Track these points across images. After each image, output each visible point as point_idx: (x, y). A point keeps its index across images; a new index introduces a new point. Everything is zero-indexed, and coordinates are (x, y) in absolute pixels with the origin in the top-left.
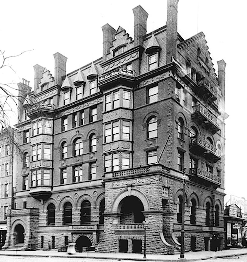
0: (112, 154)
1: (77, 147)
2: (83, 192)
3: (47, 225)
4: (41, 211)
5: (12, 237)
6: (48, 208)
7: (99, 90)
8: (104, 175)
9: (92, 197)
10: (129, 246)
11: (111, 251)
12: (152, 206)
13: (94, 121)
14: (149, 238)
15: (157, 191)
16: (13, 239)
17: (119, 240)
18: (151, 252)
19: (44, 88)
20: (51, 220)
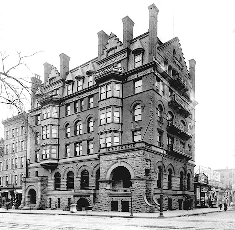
1: (78, 128)
4: (49, 178)
5: (27, 199)
7: (95, 83)
9: (90, 167)
10: (119, 206)
12: (137, 175)
15: (141, 163)
16: (27, 201)
17: (111, 201)
18: (136, 210)
19: (52, 81)
20: (57, 186)
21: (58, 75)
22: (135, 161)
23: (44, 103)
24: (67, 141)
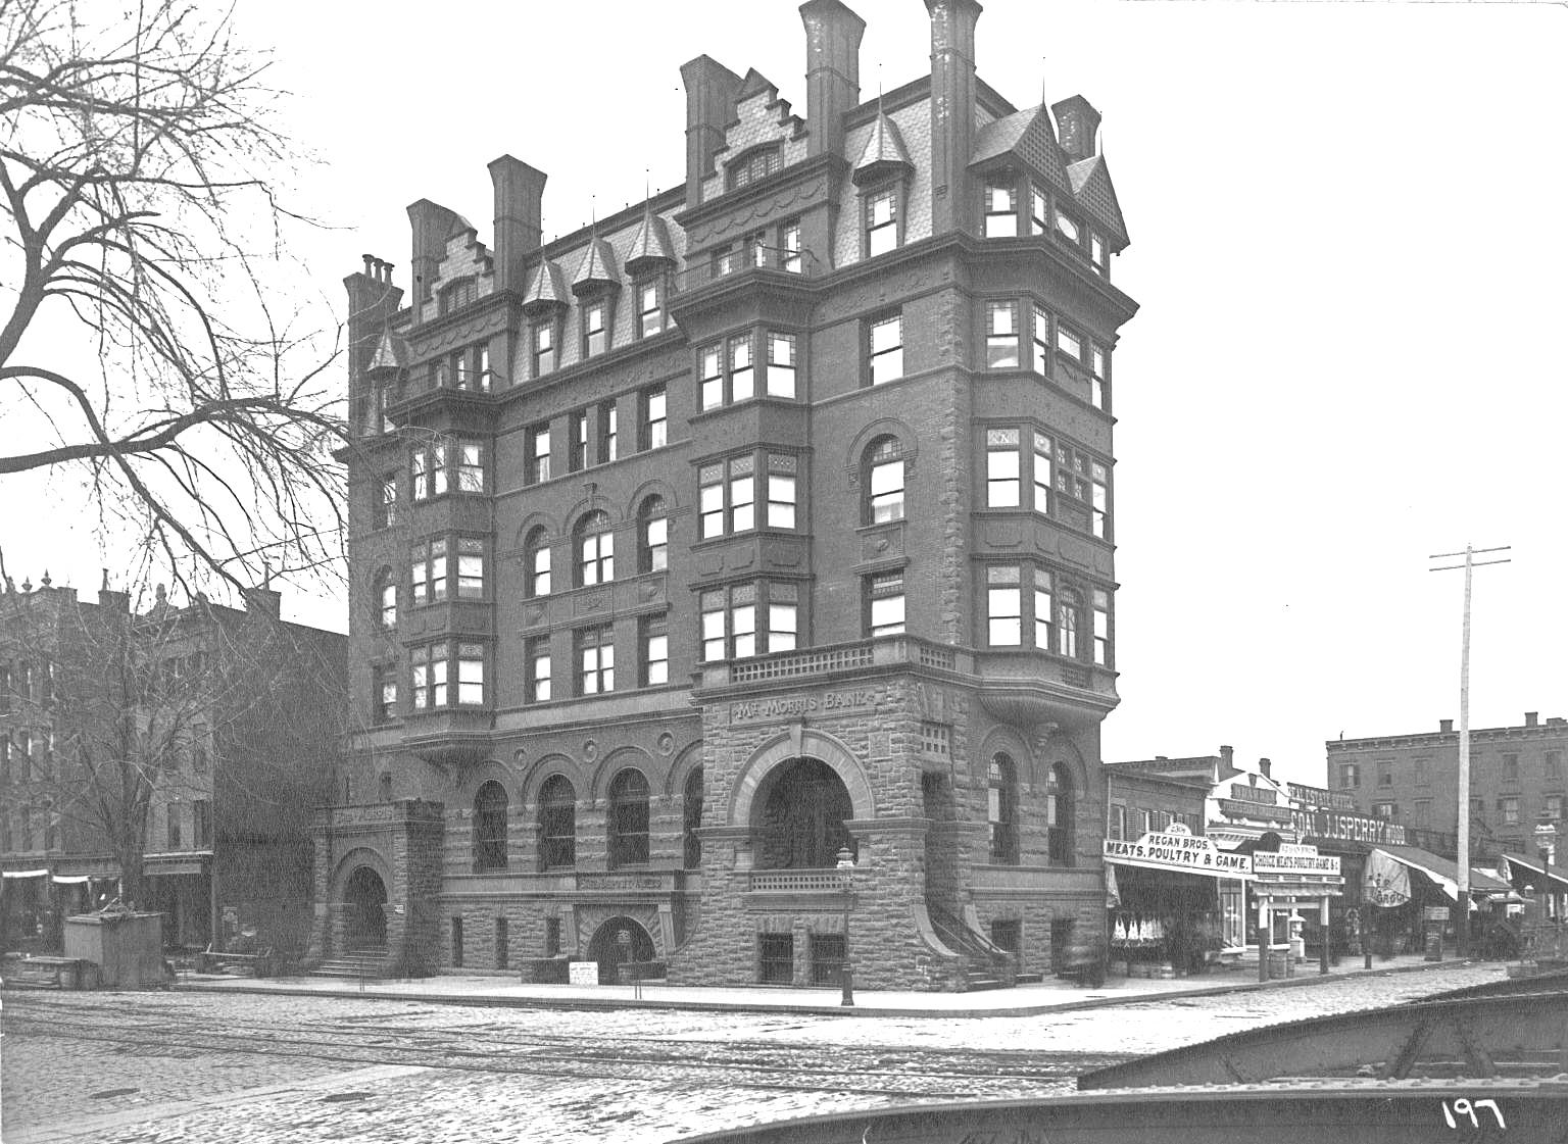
0: (726, 588)
1: (589, 550)
2: (617, 740)
3: (475, 871)
4: (449, 813)
5: (338, 924)
6: (478, 804)
7: (672, 324)
8: (698, 671)
9: (652, 756)
11: (729, 976)
13: (655, 445)
14: (860, 929)
17: (761, 936)
20: (491, 856)
21: (482, 267)
22: (872, 731)
23: (418, 416)
24: (536, 619)
